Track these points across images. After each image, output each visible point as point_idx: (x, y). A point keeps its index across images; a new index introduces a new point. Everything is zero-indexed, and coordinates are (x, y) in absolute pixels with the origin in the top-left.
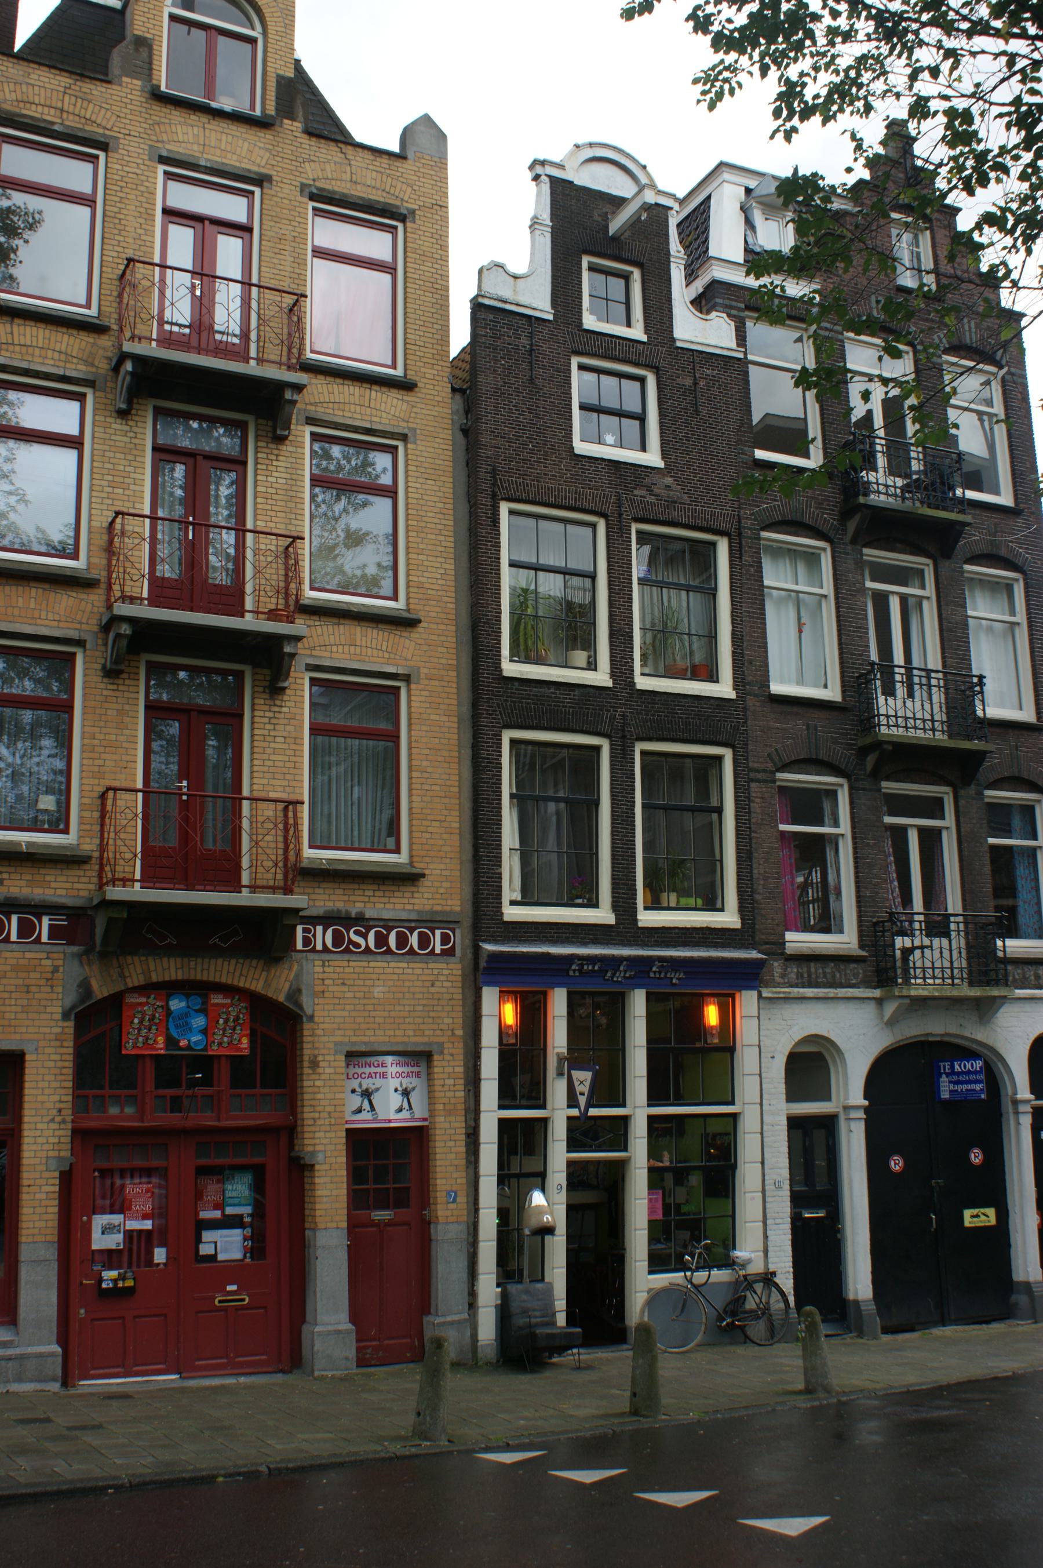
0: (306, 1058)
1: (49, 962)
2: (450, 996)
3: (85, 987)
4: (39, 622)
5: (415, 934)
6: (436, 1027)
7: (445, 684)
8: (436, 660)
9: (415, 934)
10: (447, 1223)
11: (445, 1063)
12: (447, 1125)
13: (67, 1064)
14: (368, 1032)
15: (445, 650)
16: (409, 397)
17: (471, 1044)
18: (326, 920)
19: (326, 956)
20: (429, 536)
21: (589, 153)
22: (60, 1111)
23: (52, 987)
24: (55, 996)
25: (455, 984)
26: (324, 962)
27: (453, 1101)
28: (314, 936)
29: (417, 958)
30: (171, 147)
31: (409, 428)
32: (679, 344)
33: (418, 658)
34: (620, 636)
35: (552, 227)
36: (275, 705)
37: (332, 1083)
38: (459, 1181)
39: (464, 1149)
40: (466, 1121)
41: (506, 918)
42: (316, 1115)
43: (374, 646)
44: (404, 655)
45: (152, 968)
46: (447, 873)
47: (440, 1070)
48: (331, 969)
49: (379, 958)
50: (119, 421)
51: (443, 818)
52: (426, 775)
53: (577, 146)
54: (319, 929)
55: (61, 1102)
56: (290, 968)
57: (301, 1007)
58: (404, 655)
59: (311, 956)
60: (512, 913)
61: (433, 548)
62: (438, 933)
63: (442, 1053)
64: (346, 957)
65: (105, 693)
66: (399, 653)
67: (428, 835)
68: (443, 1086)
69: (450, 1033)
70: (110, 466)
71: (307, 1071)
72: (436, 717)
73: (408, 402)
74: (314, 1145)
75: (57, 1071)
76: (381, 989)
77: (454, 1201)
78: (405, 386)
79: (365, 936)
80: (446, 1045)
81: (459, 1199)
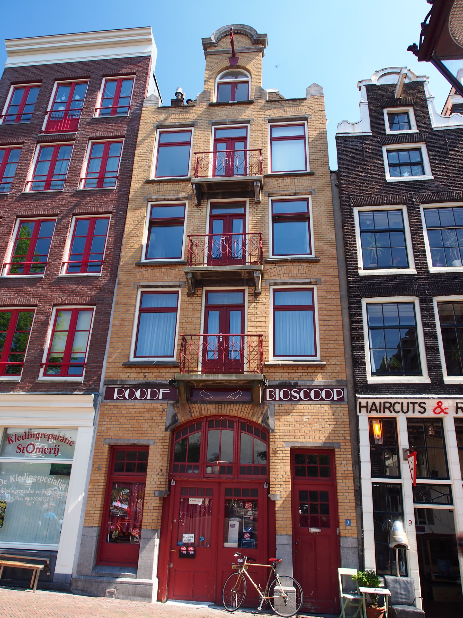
1: (161, 407)
3: (175, 416)
4: (164, 280)
5: (324, 391)
6: (336, 435)
7: (334, 283)
8: (329, 274)
9: (324, 391)
10: (346, 537)
11: (341, 453)
12: (344, 485)
13: (166, 450)
16: (312, 178)
18: (280, 386)
20: (323, 227)
22: (161, 470)
23: (162, 417)
24: (162, 421)
25: (345, 414)
26: (279, 405)
27: (346, 472)
28: (275, 393)
29: (325, 402)
30: (217, 119)
31: (312, 189)
32: (435, 130)
33: (320, 275)
35: (368, 102)
36: (257, 300)
38: (352, 514)
39: (354, 498)
41: (369, 383)
42: (276, 476)
44: (314, 274)
46: (338, 363)
47: (339, 456)
48: (283, 408)
49: (306, 403)
50: (196, 209)
51: (335, 339)
53: (377, 72)
54: (277, 390)
55: (162, 466)
56: (264, 408)
57: (268, 425)
59: (273, 402)
60: (372, 379)
61: (325, 231)
62: (335, 391)
63: (339, 448)
64: (290, 402)
65: (188, 302)
67: (328, 347)
68: (341, 464)
69: (343, 438)
70: (193, 224)
71: (271, 455)
72: (330, 297)
73: (311, 180)
74: (275, 491)
75: (161, 453)
76: (307, 417)
77: (349, 525)
78: (311, 174)
79: (299, 393)
80: (341, 444)
81: (352, 524)
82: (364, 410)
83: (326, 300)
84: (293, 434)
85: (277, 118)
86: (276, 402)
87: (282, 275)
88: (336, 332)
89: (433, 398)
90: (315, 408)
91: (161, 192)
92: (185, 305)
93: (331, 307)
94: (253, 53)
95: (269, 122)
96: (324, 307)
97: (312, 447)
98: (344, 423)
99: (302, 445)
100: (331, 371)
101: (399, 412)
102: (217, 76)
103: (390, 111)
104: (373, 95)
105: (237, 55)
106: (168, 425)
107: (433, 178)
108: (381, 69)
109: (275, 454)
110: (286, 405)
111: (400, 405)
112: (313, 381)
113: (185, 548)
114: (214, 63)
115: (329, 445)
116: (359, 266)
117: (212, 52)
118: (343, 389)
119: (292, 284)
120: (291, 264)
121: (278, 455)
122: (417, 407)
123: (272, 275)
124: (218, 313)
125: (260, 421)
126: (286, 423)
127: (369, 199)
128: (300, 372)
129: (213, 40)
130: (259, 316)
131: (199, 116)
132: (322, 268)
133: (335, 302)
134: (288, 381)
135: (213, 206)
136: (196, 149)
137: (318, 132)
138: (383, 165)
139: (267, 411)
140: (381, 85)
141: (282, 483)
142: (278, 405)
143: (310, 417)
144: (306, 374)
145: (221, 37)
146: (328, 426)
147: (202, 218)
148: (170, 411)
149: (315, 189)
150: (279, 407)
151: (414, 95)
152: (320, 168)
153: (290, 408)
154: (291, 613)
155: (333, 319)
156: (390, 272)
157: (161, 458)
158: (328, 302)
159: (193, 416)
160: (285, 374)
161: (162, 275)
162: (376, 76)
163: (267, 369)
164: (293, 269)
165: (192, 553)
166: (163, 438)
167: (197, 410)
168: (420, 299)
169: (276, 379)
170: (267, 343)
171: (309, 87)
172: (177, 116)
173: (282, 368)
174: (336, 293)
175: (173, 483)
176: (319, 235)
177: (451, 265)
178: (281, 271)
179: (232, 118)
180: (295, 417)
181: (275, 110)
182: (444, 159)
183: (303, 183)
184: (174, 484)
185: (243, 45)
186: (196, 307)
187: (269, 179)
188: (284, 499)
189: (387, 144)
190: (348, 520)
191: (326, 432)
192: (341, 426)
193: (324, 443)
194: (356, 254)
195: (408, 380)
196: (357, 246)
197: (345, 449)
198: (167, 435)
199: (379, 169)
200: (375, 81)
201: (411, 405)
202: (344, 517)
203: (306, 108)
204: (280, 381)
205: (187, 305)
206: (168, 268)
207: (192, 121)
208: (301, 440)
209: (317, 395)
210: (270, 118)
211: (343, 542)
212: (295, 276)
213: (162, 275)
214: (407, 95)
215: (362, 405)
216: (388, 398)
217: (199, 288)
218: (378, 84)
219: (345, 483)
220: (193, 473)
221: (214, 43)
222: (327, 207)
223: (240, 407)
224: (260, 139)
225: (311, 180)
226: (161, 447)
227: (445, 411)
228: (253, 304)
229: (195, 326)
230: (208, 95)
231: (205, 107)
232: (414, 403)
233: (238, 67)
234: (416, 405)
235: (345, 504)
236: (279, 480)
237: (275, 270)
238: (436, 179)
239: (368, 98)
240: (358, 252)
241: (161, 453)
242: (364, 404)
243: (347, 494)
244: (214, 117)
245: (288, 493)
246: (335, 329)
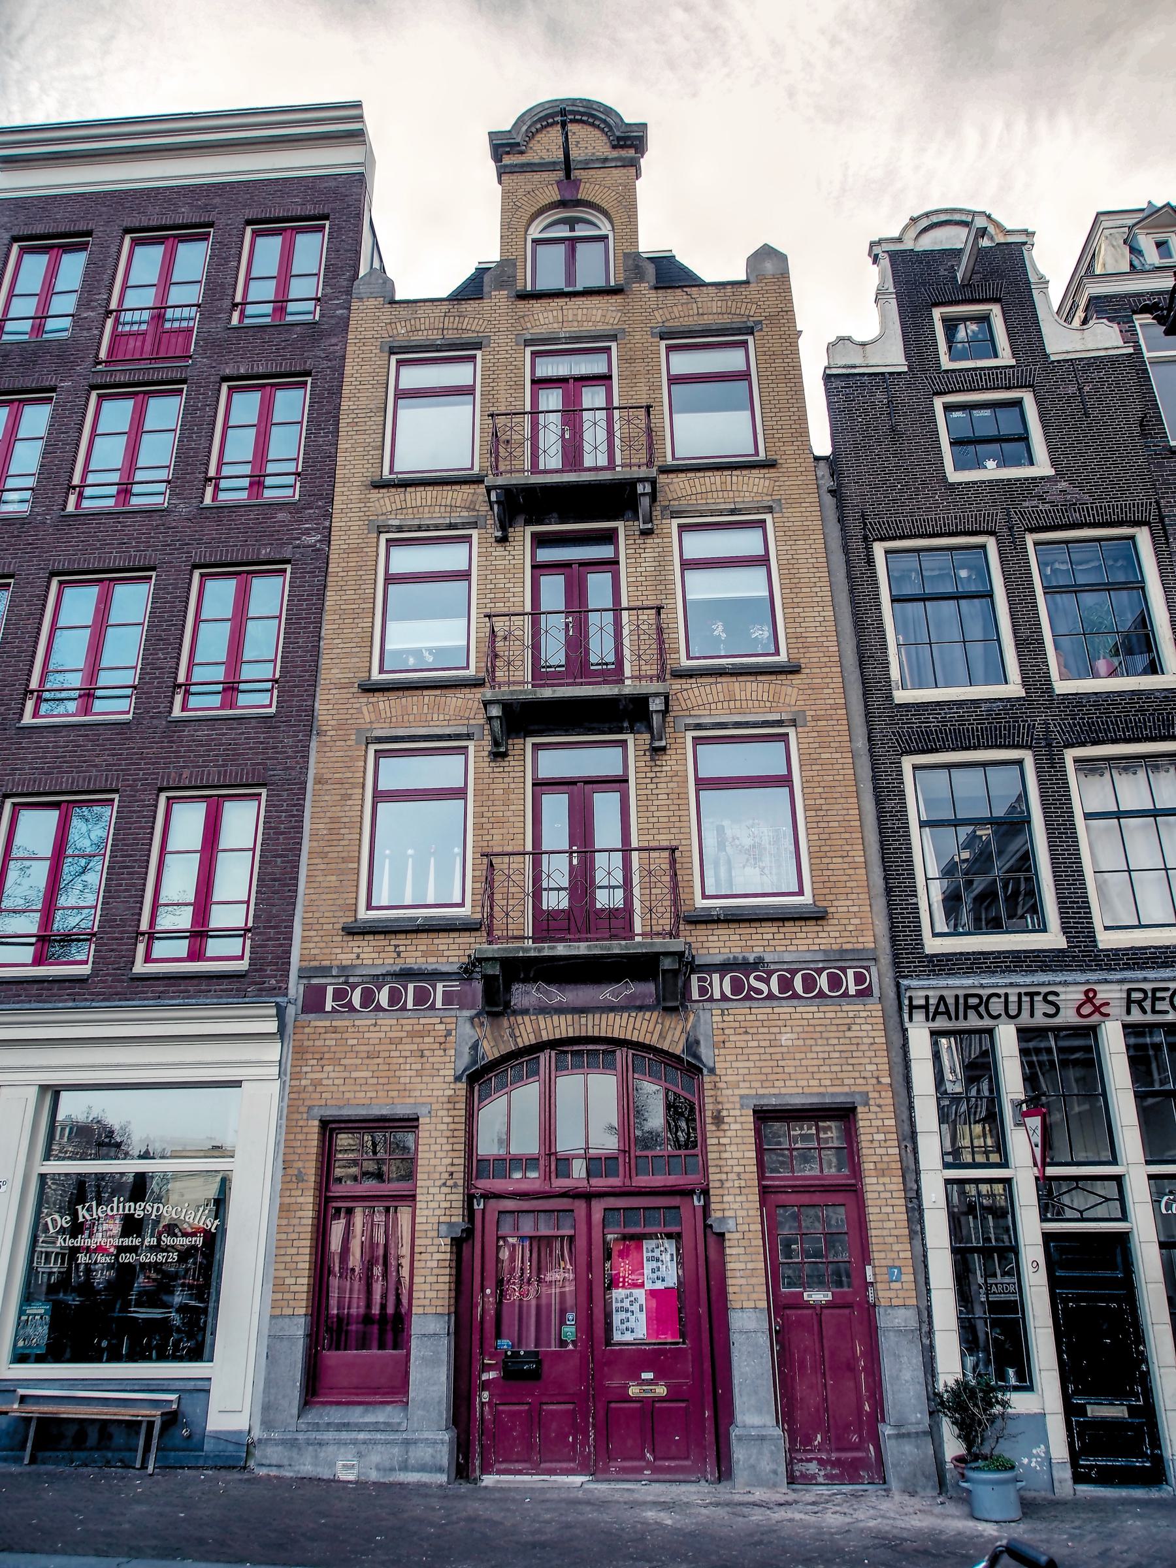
1: (442, 1027)
2: (871, 1040)
3: (475, 1047)
4: (431, 723)
7: (835, 722)
9: (824, 975)
12: (881, 1188)
19: (725, 1005)
21: (925, 223)
22: (452, 1174)
23: (445, 1050)
24: (448, 1059)
27: (885, 1159)
28: (711, 984)
32: (1053, 358)
33: (802, 703)
34: (1029, 644)
35: (896, 293)
38: (902, 1255)
45: (543, 1026)
48: (731, 1018)
49: (784, 1003)
55: (452, 1165)
58: (787, 701)
59: (707, 1005)
62: (850, 972)
63: (867, 1104)
64: (748, 1004)
66: (782, 701)
67: (830, 873)
68: (872, 1141)
69: (874, 1081)
72: (828, 756)
75: (449, 1134)
79: (767, 981)
80: (871, 1095)
81: (904, 1278)
82: (919, 1016)
83: (819, 762)
86: (714, 1005)
87: (713, 706)
88: (847, 836)
93: (831, 778)
95: (662, 339)
96: (816, 779)
98: (875, 1047)
107: (1052, 472)
118: (868, 969)
119: (738, 725)
121: (725, 1127)
122: (1041, 1007)
133: (840, 766)
134: (740, 957)
144: (782, 936)
145: (534, 130)
150: (723, 1014)
155: (837, 807)
157: (449, 1147)
158: (825, 767)
161: (426, 711)
167: (530, 1030)
186: (512, 786)
187: (671, 476)
190: (896, 1267)
197: (879, 1106)
201: (1025, 999)
211: (884, 1320)
212: (744, 706)
213: (426, 711)
217: (516, 741)
219: (884, 1184)
222: (811, 542)
227: (1104, 1010)
232: (1031, 995)
237: (697, 693)
241: (449, 1134)
243: (890, 1209)
244: (529, 325)
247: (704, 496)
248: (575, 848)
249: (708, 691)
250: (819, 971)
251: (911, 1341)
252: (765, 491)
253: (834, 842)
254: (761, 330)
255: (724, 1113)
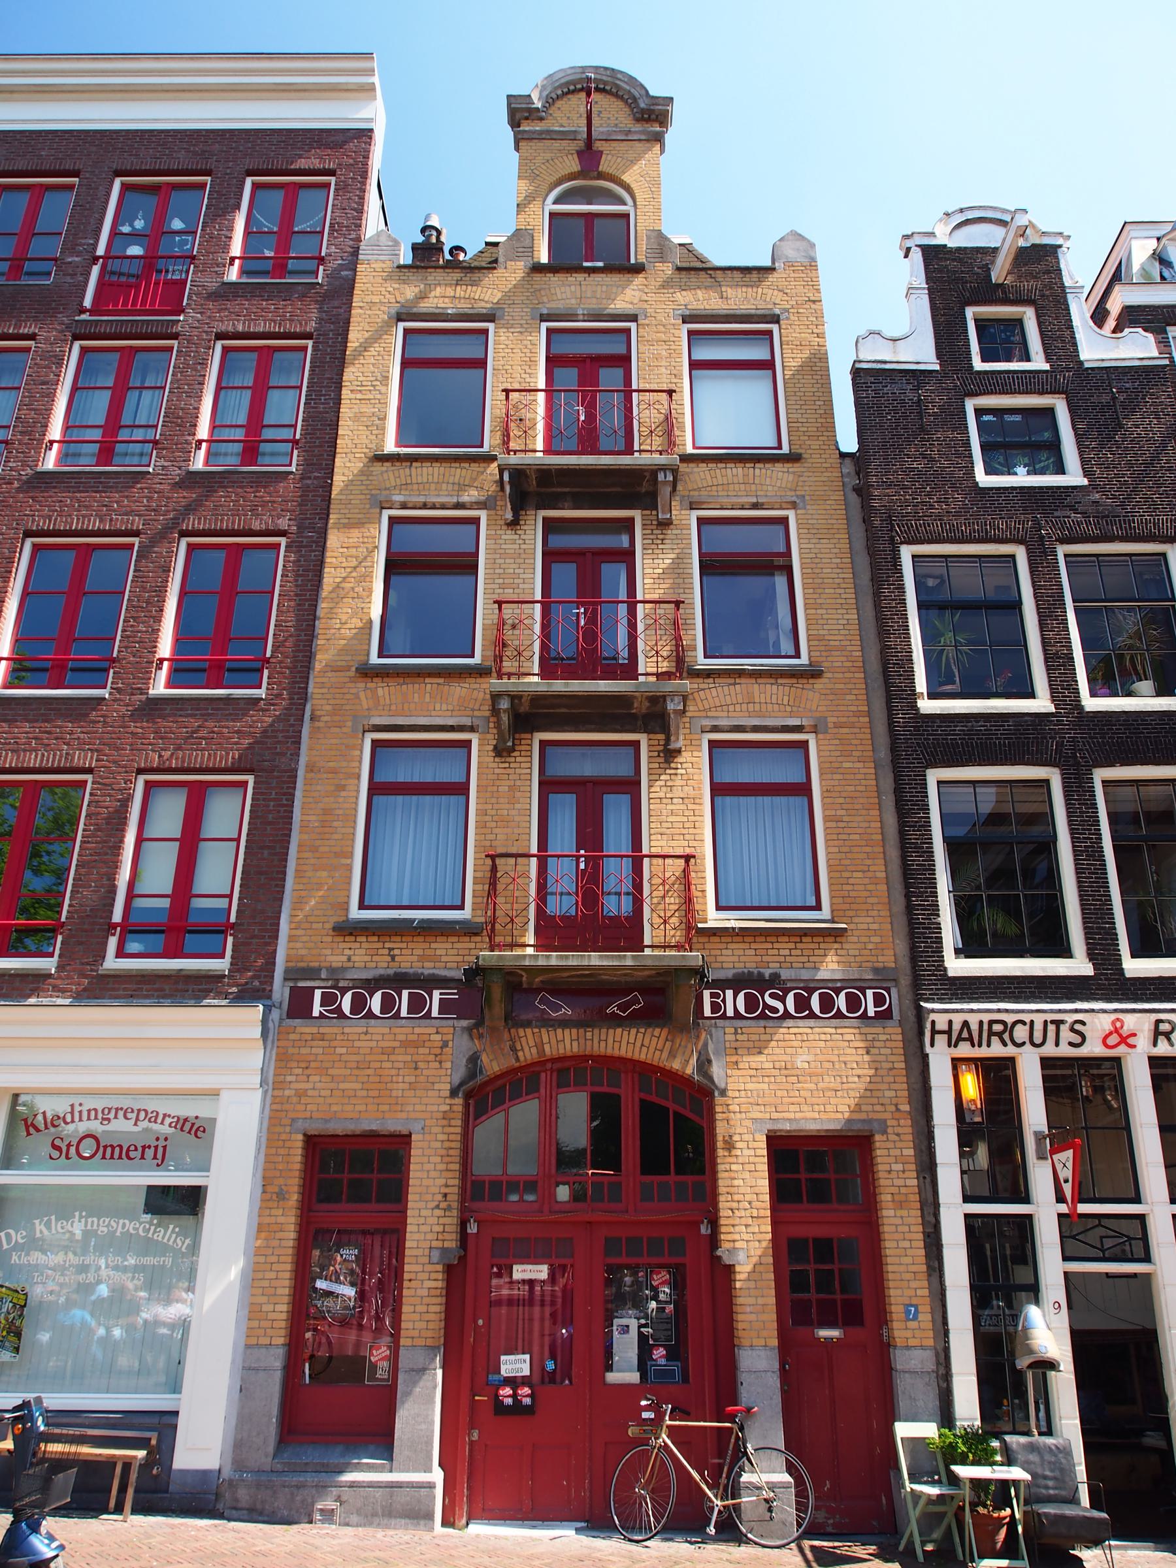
0: (720, 1138)
1: (438, 1037)
2: (891, 1065)
3: (474, 1059)
4: (433, 713)
5: (842, 995)
9: (842, 995)
10: (908, 1348)
11: (890, 1145)
12: (899, 1221)
13: (453, 1145)
14: (792, 1108)
15: (854, 697)
16: (795, 468)
17: (923, 1122)
18: (737, 983)
19: (739, 1023)
20: (827, 591)
22: (445, 1195)
23: (440, 1062)
24: (443, 1072)
25: (895, 1051)
26: (736, 1029)
27: (903, 1190)
28: (724, 1001)
29: (846, 1022)
30: (553, 305)
31: (797, 496)
32: (1087, 365)
33: (824, 708)
34: (1058, 661)
35: (929, 289)
37: (752, 1167)
38: (919, 1292)
39: (923, 1252)
40: (922, 1216)
42: (735, 1205)
43: (774, 701)
44: (808, 706)
45: (545, 1039)
46: (875, 926)
48: (744, 1037)
49: (800, 1023)
50: (509, 532)
52: (841, 825)
53: (947, 214)
54: (729, 993)
55: (447, 1186)
56: (698, 1037)
57: (711, 1079)
59: (720, 1023)
61: (833, 601)
62: (870, 993)
63: (885, 1132)
64: (762, 1023)
65: (497, 771)
66: (802, 705)
67: (849, 887)
68: (890, 1172)
69: (893, 1108)
71: (720, 1152)
73: (794, 473)
74: (734, 1241)
75: (444, 1152)
76: (805, 1058)
77: (915, 1318)
78: (793, 458)
79: (783, 1000)
80: (889, 1123)
81: (921, 1317)
82: (941, 1040)
84: (772, 1100)
85: (704, 313)
86: (727, 1023)
87: (731, 708)
88: (868, 849)
89: (1104, 1011)
90: (823, 1037)
91: (416, 487)
92: (490, 777)
93: (852, 788)
94: (637, 144)
95: (684, 322)
96: (837, 789)
97: (818, 1131)
99: (794, 1127)
100: (859, 946)
101: (1024, 1043)
102: (547, 195)
103: (981, 313)
104: (941, 271)
105: (598, 146)
106: (457, 1081)
108: (957, 207)
109: (729, 1150)
110: (754, 1029)
111: (1027, 1027)
112: (816, 969)
113: (508, 1391)
114: (539, 160)
115: (855, 1127)
116: (918, 690)
117: (534, 132)
118: (888, 990)
119: (756, 729)
120: (753, 681)
121: (738, 1152)
122: (1066, 1035)
123: (707, 707)
124: (571, 798)
125: (690, 1069)
126: (753, 1072)
127: (936, 526)
128: (784, 947)
129: (535, 101)
130: (678, 807)
131: (506, 295)
132: (828, 692)
133: (862, 776)
134: (756, 971)
135: (550, 526)
136: (501, 379)
137: (806, 354)
138: (967, 444)
139: (706, 1045)
140: (959, 249)
141: (750, 1221)
142: (733, 1030)
143: (810, 1058)
144: (799, 952)
145: (554, 96)
146: (856, 1079)
147: (523, 556)
148: (462, 1046)
149: (803, 496)
150: (736, 1033)
151: (1035, 277)
152: (815, 444)
153: (763, 1037)
154: (783, 1538)
155: (857, 819)
156: (992, 708)
157: (443, 1167)
159: (522, 1058)
160: (748, 952)
162: (946, 224)
163: (701, 940)
164: (756, 694)
165: (527, 1401)
166: (445, 1116)
167: (532, 1043)
168: (1062, 775)
169: (725, 965)
170: (700, 875)
171: (782, 240)
172: (450, 292)
173: (740, 939)
174: (865, 754)
175: (473, 1228)
176: (819, 611)
177: (1129, 694)
178: (716, 700)
179: (592, 305)
180: (775, 1058)
181: (699, 292)
182: (1110, 438)
183: (775, 479)
184: (475, 1231)
185: (613, 122)
186: (518, 783)
187: (691, 465)
188: (755, 1260)
189: (977, 395)
190: (912, 1305)
191: (852, 1093)
192: (886, 1079)
193: (849, 1121)
194: (910, 660)
195: (1043, 969)
196: (912, 640)
197: (898, 1135)
198: (455, 1108)
199: (958, 455)
200: (943, 237)
201: (1051, 1028)
202: (900, 1300)
203: (776, 293)
204: (735, 971)
205: (495, 777)
206: (441, 681)
207: (489, 306)
208: (792, 1116)
209: (827, 1003)
210: (688, 313)
212: (764, 709)
213: (427, 699)
214: (1020, 277)
215: (938, 1027)
216: (999, 1011)
217: (523, 736)
218: (952, 243)
220: (521, 1200)
221: (537, 109)
223: (640, 1036)
224: (664, 363)
225: (794, 473)
226: (441, 1137)
227: (1131, 1041)
228: (662, 777)
229: (516, 831)
230: (527, 243)
231: (520, 274)
232: (1058, 1023)
233: (601, 176)
234: (1064, 1029)
235: (902, 1268)
236: (743, 1213)
238: (1093, 486)
239: (928, 279)
240: (915, 655)
241: (444, 1152)
242: (942, 1025)
243: (907, 1244)
245: (764, 1244)
246: (864, 843)
247: (726, 487)
248: (582, 852)
249: (727, 692)
250: (837, 991)
251: (927, 1384)
252: (789, 485)
253: (855, 856)
254: (788, 319)
255: (736, 1138)
